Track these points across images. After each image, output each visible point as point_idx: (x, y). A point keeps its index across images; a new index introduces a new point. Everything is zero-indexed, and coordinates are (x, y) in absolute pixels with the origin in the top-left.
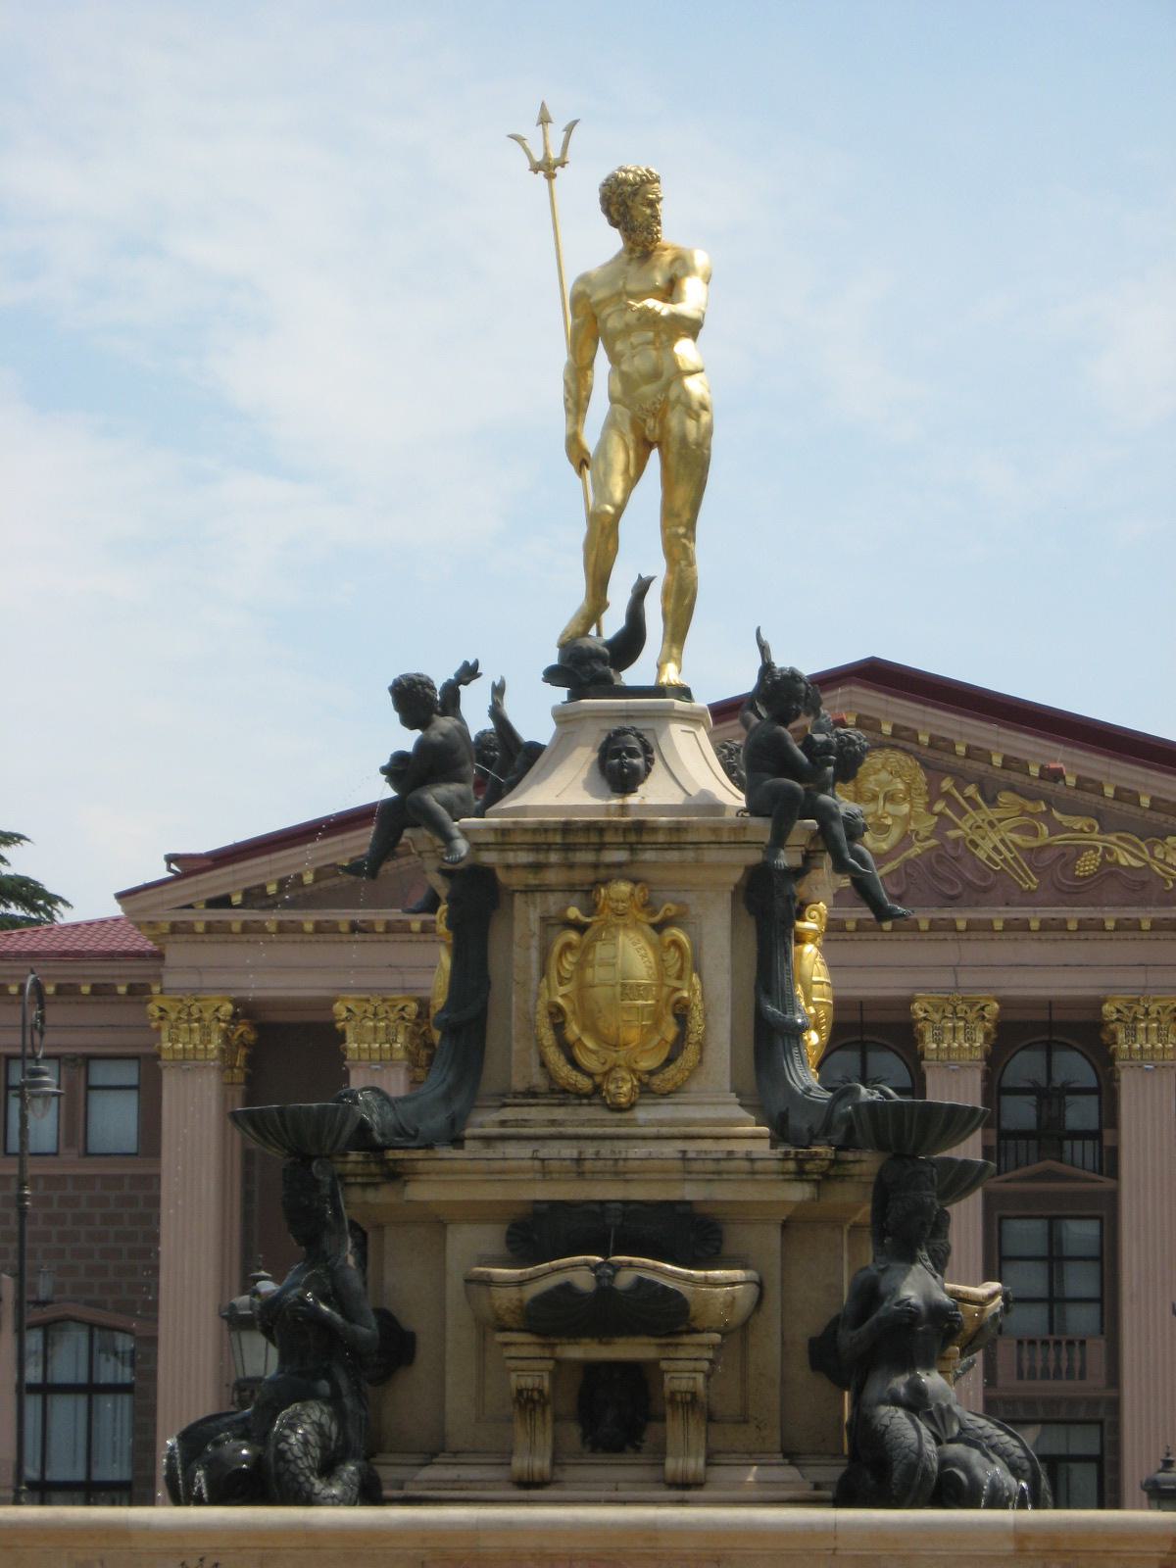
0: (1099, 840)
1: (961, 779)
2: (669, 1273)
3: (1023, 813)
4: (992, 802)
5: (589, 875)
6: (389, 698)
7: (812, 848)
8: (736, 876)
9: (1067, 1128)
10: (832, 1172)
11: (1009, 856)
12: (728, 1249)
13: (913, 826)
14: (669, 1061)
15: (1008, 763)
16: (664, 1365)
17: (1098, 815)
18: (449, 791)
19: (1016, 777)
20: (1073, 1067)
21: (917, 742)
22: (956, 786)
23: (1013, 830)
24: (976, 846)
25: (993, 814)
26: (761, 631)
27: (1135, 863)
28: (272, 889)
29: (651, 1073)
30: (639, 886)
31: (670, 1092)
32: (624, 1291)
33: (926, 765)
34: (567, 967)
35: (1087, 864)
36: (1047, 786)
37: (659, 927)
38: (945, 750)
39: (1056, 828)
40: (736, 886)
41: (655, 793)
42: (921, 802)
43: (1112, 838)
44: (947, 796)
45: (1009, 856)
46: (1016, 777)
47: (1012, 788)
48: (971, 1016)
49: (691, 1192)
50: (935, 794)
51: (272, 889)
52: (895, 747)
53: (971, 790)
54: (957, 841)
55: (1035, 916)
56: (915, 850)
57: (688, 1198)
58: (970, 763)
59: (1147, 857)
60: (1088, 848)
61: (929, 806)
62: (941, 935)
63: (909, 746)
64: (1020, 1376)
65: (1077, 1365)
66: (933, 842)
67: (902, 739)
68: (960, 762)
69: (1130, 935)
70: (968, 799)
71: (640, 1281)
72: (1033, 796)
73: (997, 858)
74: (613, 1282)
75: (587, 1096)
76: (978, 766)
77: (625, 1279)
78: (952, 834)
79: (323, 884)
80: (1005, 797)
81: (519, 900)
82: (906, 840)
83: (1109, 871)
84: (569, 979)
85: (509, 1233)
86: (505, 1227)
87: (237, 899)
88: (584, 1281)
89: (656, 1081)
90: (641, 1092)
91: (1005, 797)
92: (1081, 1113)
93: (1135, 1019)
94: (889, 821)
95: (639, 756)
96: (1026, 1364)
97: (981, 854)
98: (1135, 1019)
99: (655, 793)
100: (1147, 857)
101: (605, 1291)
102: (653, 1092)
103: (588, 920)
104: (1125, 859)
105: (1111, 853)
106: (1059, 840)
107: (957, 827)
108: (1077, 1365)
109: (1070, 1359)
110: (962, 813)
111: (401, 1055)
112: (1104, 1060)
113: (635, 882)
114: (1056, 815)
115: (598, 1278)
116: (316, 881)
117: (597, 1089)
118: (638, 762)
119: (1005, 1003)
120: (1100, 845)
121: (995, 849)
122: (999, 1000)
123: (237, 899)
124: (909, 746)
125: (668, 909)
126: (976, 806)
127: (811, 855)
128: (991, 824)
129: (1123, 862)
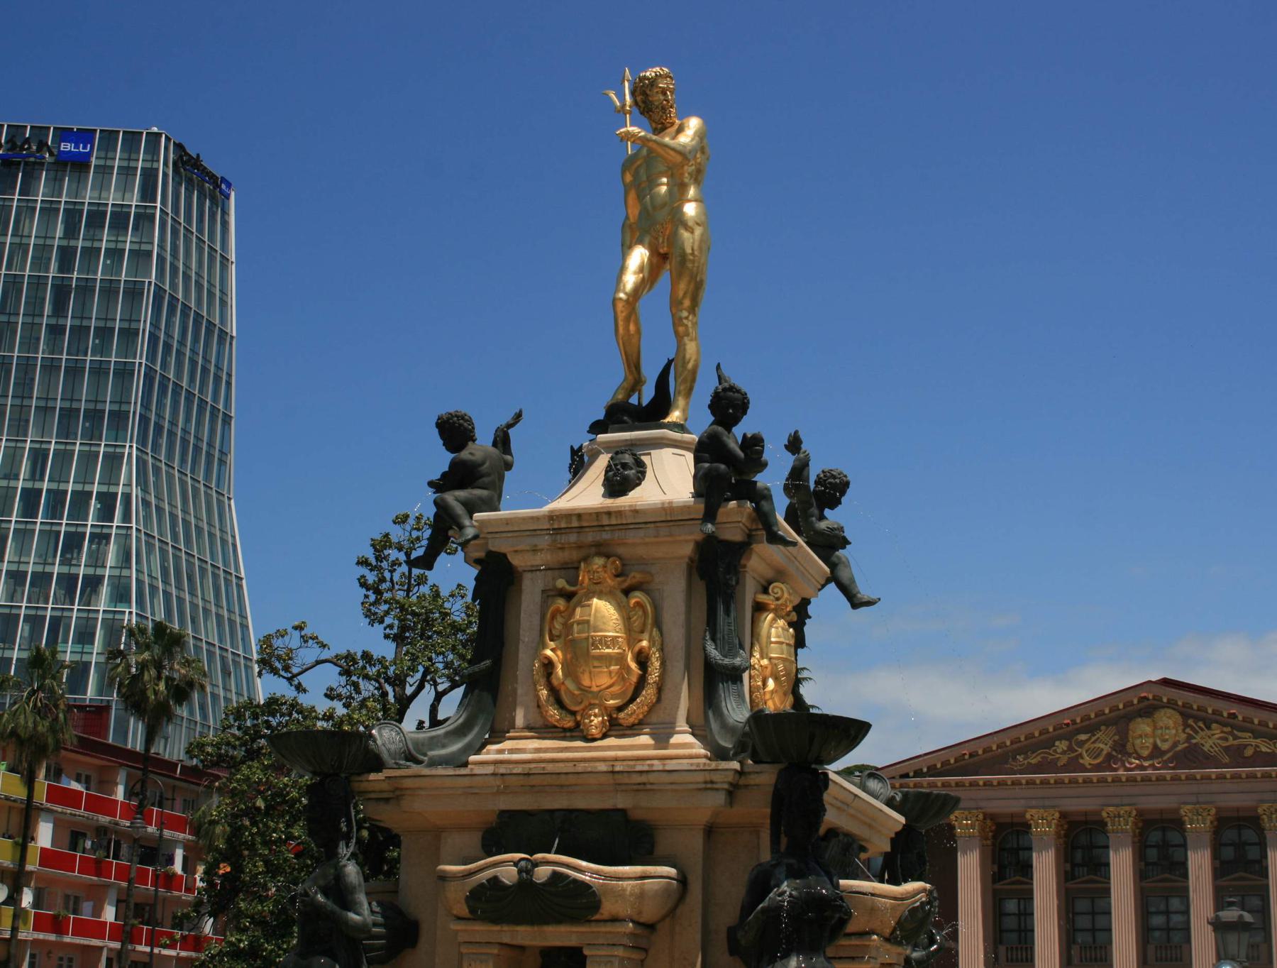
0: (1254, 742)
1: (1197, 719)
2: (586, 871)
3: (1222, 732)
4: (1209, 728)
5: (575, 555)
6: (436, 431)
7: (754, 527)
8: (688, 550)
9: (480, 568)
10: (741, 782)
11: (1217, 749)
12: (661, 848)
13: (1177, 738)
14: (632, 700)
15: (1214, 712)
16: (586, 952)
17: (1252, 731)
18: (471, 494)
19: (1218, 718)
20: (1249, 835)
21: (1178, 705)
22: (1194, 722)
23: (1219, 739)
24: (1204, 746)
25: (1209, 733)
26: (722, 366)
27: (1269, 751)
28: (925, 770)
29: (620, 709)
30: (611, 559)
31: (633, 725)
32: (543, 884)
33: (1182, 714)
34: (557, 627)
35: (1249, 752)
36: (1231, 721)
37: (627, 592)
38: (1188, 708)
39: (1236, 738)
40: (691, 560)
41: (645, 495)
42: (1180, 728)
43: (1258, 741)
44: (1190, 726)
45: (1217, 749)
46: (1218, 718)
47: (1217, 722)
48: (1205, 814)
49: (621, 802)
50: (1186, 725)
51: (925, 770)
52: (1168, 707)
53: (1201, 724)
54: (1195, 744)
55: (1227, 771)
56: (1180, 747)
57: (620, 806)
58: (1199, 713)
59: (1273, 748)
60: (1248, 745)
61: (1184, 731)
62: (1191, 782)
63: (1174, 706)
64: (1157, 961)
65: (1179, 956)
66: (1186, 745)
67: (1171, 704)
68: (1195, 712)
69: (1267, 779)
70: (1200, 727)
71: (555, 873)
72: (1225, 725)
73: (1212, 750)
74: (532, 876)
75: (570, 730)
76: (1203, 714)
77: (542, 873)
78: (1194, 741)
79: (945, 768)
80: (1214, 726)
81: (527, 576)
82: (1175, 744)
83: (1257, 753)
84: (559, 637)
85: (483, 838)
86: (480, 834)
87: (911, 774)
88: (508, 874)
89: (624, 717)
90: (611, 725)
91: (1214, 726)
92: (1253, 853)
93: (1272, 813)
94: (1167, 737)
95: (631, 469)
96: (1159, 955)
97: (1205, 749)
98: (1272, 813)
99: (645, 495)
100: (1273, 748)
101: (525, 884)
102: (621, 725)
103: (573, 589)
104: (1264, 749)
105: (1258, 747)
106: (1236, 742)
107: (1195, 738)
108: (1179, 956)
109: (1166, 954)
110: (1197, 732)
111: (977, 834)
112: (1260, 831)
113: (608, 556)
114: (1235, 732)
115: (520, 872)
116: (942, 766)
117: (578, 724)
118: (631, 473)
119: (1219, 810)
120: (1253, 744)
121: (1211, 746)
122: (1216, 808)
123: (911, 774)
124: (1174, 706)
125: (635, 577)
126: (1202, 730)
127: (754, 533)
128: (1209, 737)
129: (1263, 750)
